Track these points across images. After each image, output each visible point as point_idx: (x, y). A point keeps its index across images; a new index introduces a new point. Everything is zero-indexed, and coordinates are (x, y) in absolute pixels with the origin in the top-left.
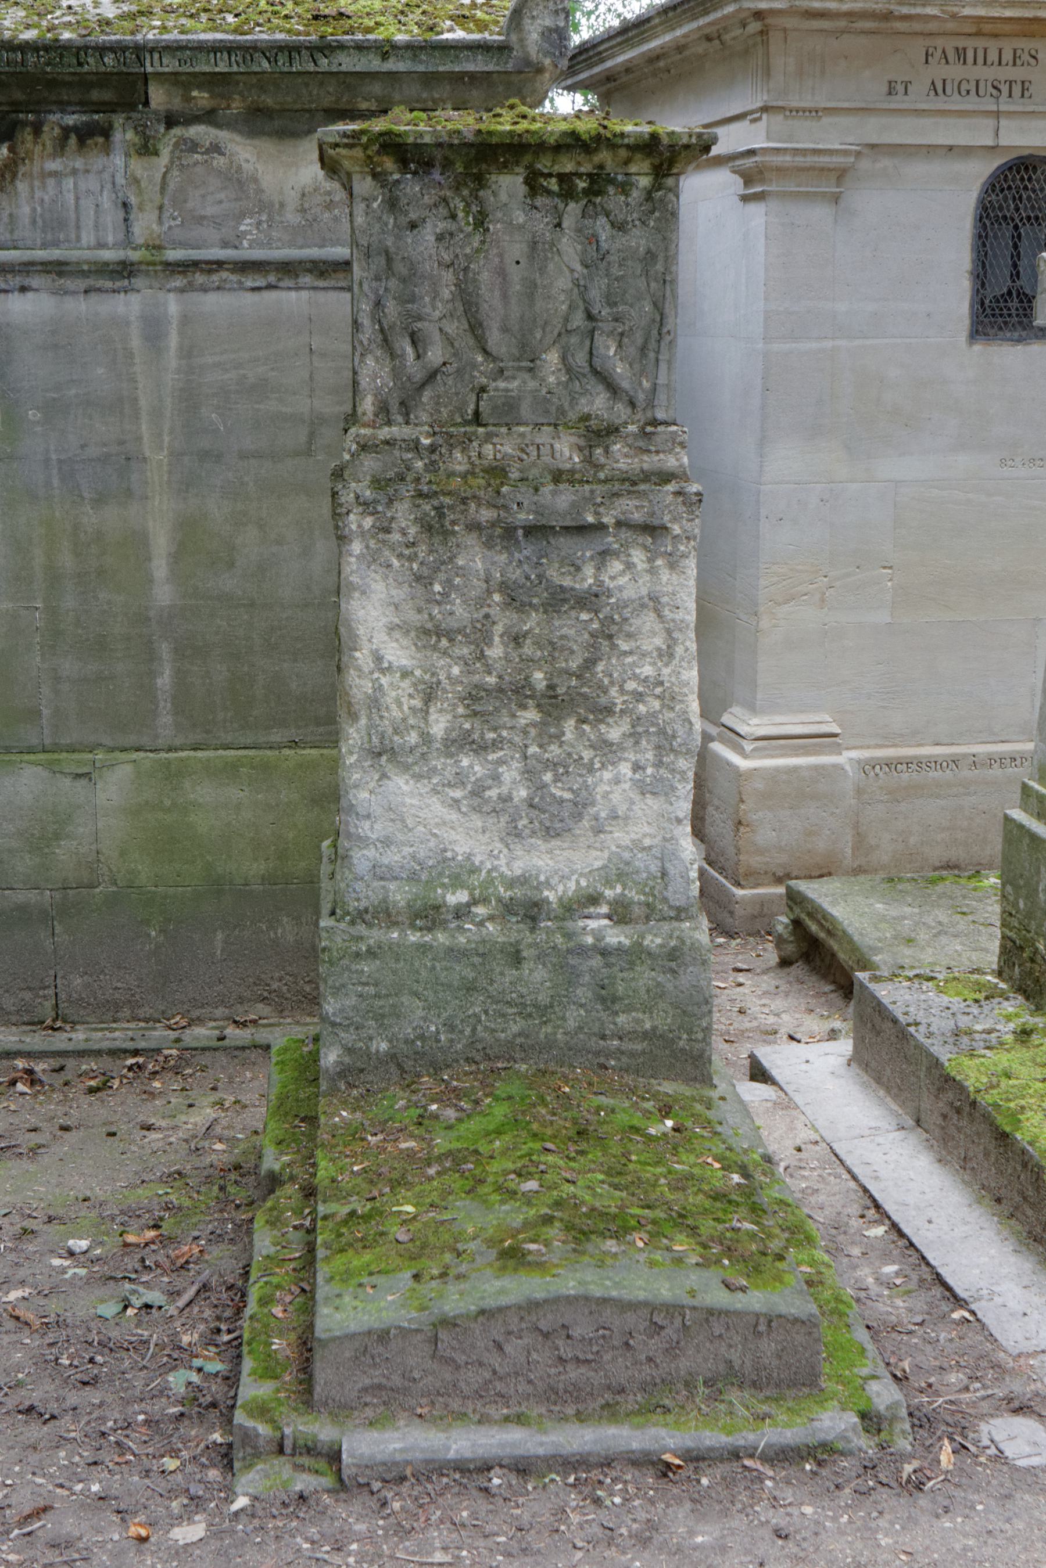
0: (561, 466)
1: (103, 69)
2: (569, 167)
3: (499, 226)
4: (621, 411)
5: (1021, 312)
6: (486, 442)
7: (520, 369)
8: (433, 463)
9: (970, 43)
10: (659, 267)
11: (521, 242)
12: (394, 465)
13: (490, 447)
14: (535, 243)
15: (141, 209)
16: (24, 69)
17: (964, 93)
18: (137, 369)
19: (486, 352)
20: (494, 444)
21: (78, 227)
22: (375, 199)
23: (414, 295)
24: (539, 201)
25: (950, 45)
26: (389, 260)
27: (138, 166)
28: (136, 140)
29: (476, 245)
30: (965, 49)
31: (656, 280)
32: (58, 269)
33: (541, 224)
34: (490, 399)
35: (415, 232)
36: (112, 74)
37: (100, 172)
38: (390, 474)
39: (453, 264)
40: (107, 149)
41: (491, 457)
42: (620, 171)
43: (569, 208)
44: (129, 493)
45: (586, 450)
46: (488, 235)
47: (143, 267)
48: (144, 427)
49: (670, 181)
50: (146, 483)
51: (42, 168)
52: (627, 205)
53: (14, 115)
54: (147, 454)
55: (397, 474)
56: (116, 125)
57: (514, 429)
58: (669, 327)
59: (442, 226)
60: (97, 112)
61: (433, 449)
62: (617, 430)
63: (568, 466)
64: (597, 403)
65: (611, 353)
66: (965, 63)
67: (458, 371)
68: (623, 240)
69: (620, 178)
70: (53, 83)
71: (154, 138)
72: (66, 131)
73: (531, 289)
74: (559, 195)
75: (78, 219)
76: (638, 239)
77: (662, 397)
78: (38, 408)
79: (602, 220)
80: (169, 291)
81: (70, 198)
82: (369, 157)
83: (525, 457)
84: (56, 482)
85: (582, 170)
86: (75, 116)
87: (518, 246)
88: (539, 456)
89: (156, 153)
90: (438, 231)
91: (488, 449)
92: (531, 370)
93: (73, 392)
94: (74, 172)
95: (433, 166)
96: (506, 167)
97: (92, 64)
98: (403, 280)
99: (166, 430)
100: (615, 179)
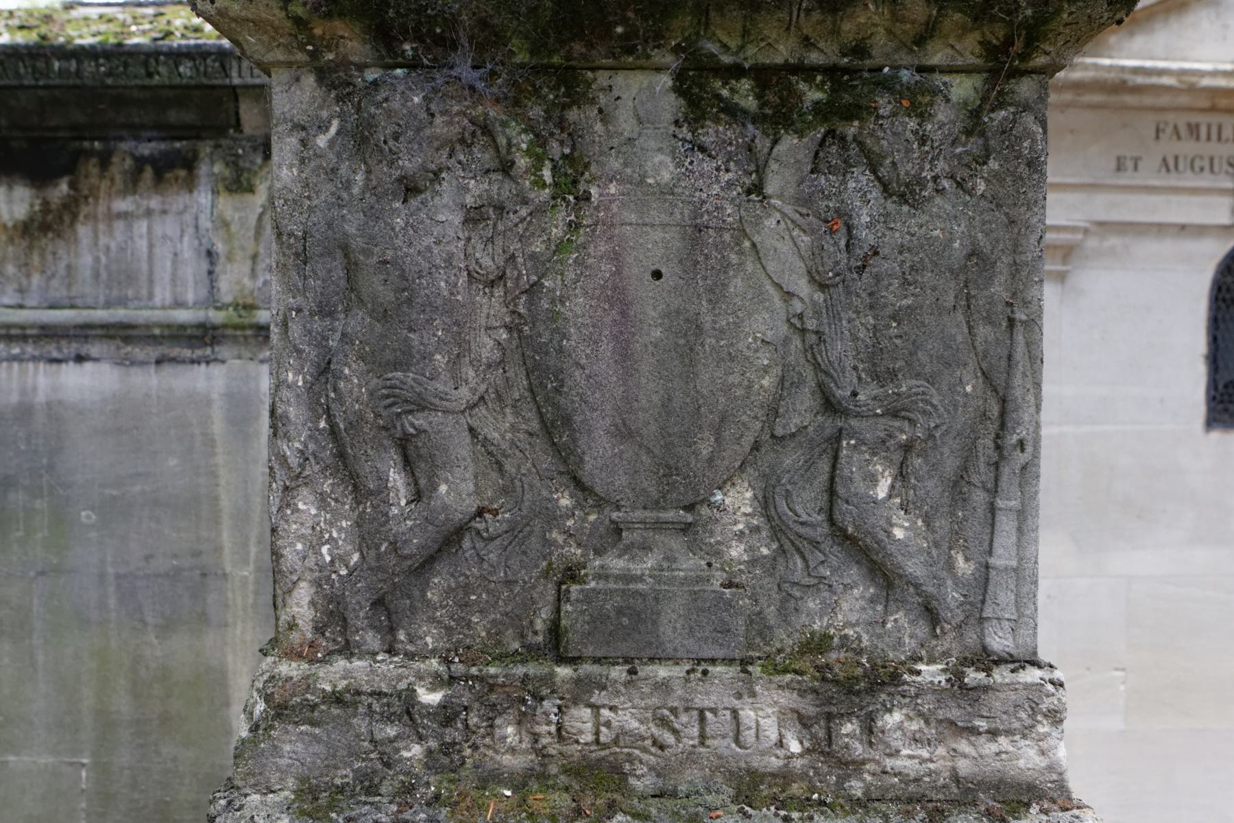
0: (756, 763)
1: (177, 81)
2: (783, 52)
3: (613, 189)
4: (904, 627)
5: (1226, 397)
6: (575, 702)
7: (659, 526)
8: (448, 748)
9: (1202, 119)
10: (999, 289)
11: (664, 226)
12: (355, 754)
13: (587, 713)
14: (699, 229)
15: (230, 258)
16: (78, 82)
17: (1197, 169)
18: (220, 459)
19: (579, 485)
20: (595, 708)
21: (151, 282)
22: (323, 127)
23: (407, 350)
24: (710, 134)
25: (1182, 120)
26: (352, 269)
27: (227, 205)
28: (227, 173)
29: (556, 232)
30: (1198, 126)
31: (989, 320)
32: (123, 333)
33: (716, 184)
34: (588, 597)
35: (414, 203)
36: (187, 87)
37: (180, 213)
38: (344, 775)
39: (502, 277)
40: (190, 185)
41: (589, 738)
42: (905, 59)
43: (781, 148)
44: (203, 618)
45: (819, 725)
46: (587, 211)
47: (229, 332)
48: (225, 535)
49: (1025, 88)
50: (226, 605)
51: (109, 209)
52: (923, 141)
53: (77, 144)
54: (228, 569)
55: (361, 776)
56: (202, 155)
57: (645, 670)
58: (1022, 432)
59: (476, 189)
60: (180, 139)
61: (447, 714)
62: (895, 678)
63: (775, 763)
64: (847, 610)
65: (882, 492)
66: (1198, 138)
67: (512, 529)
68: (908, 225)
69: (905, 75)
70: (120, 100)
71: (249, 170)
72: (140, 162)
73: (688, 335)
74: (757, 119)
75: (151, 273)
76: (947, 223)
77: (1003, 596)
78: (92, 509)
79: (860, 178)
80: (262, 362)
81: (142, 244)
82: (298, 21)
83: (669, 738)
84: (112, 602)
85: (814, 58)
86: (153, 144)
87: (658, 235)
88: (703, 737)
89: (251, 190)
90: (469, 200)
91: (581, 719)
92: (686, 528)
93: (138, 488)
94: (149, 213)
95: (454, 46)
96: (630, 51)
97: (162, 76)
98: (383, 316)
99: (253, 540)
100: (895, 78)
